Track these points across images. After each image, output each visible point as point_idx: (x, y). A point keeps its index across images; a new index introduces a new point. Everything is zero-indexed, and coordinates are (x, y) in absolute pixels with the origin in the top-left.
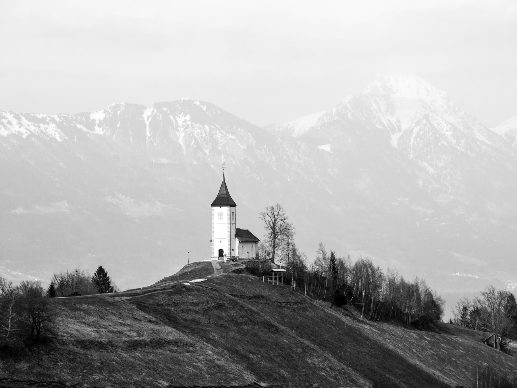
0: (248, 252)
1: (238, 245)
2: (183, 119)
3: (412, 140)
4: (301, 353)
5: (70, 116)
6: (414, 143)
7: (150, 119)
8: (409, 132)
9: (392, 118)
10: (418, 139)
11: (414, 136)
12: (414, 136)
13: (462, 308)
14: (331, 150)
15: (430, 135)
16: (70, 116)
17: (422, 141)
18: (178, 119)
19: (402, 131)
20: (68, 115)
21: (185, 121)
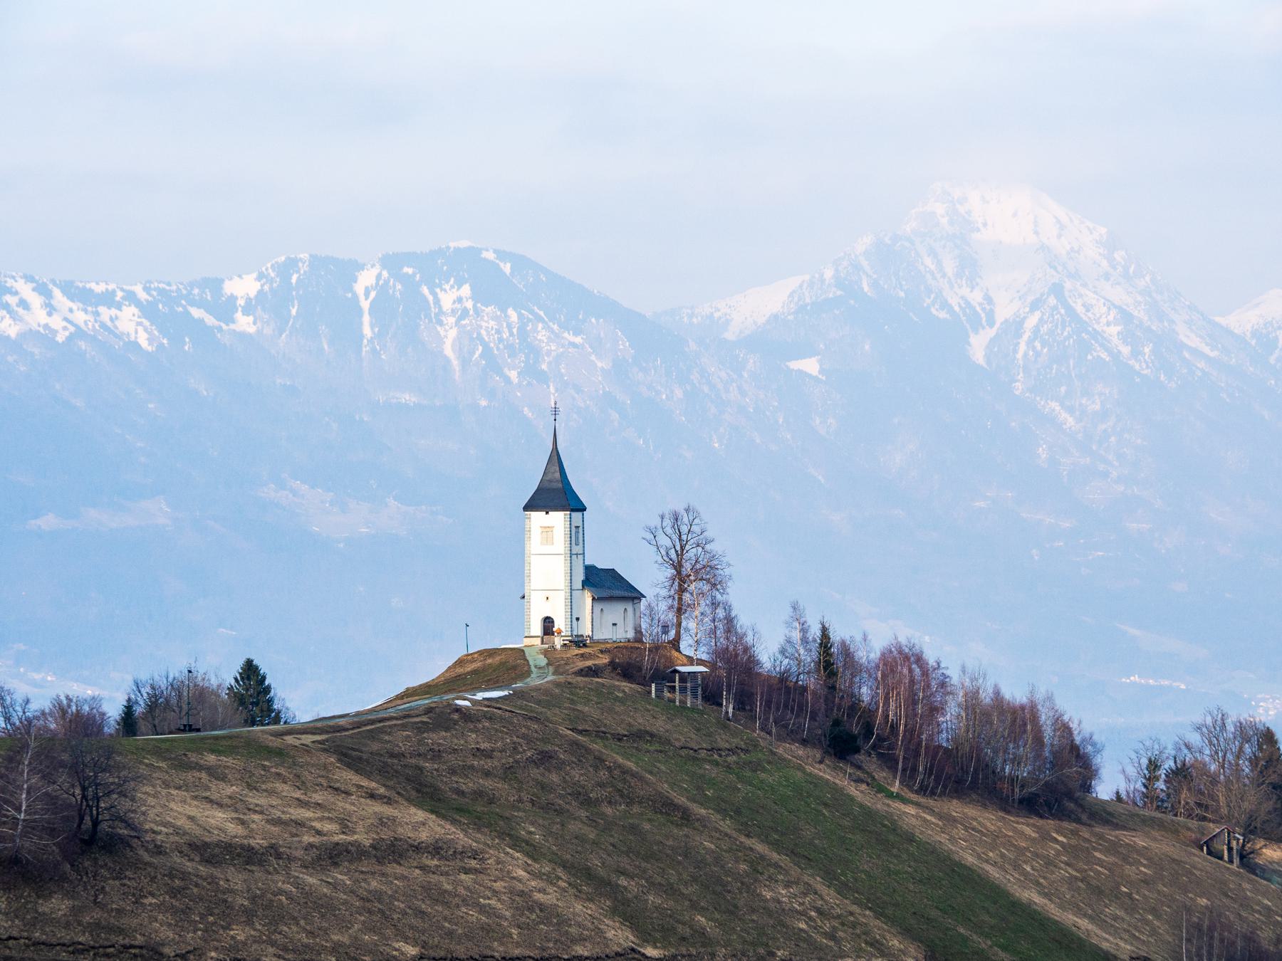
3: (1022, 348)
5: (174, 288)
6: (1026, 355)
7: (373, 294)
8: (1016, 326)
10: (1038, 345)
11: (1025, 337)
12: (1025, 337)
13: (1145, 762)
14: (820, 372)
15: (1066, 334)
16: (174, 288)
17: (1045, 350)
18: (441, 295)
21: (460, 300)
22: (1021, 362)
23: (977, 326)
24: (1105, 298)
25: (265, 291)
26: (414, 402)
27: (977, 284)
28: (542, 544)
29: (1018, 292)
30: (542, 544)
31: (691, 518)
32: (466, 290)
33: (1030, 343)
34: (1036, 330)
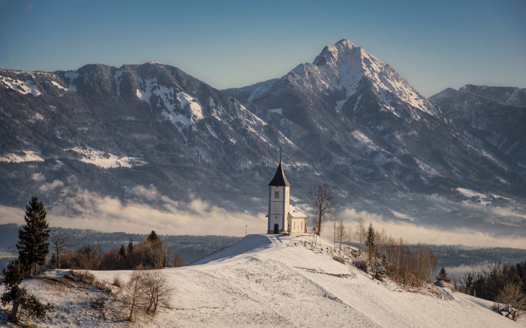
0: (298, 227)
1: (334, 274)
2: (151, 81)
3: (356, 106)
4: (200, 180)
5: (46, 74)
6: (357, 109)
7: (121, 80)
8: (353, 99)
9: (338, 86)
10: (361, 106)
11: (357, 103)
12: (357, 103)
13: (467, 277)
14: (282, 114)
15: (372, 102)
16: (46, 74)
17: (364, 108)
18: (146, 81)
19: (347, 98)
20: (44, 72)
21: (153, 83)
22: (355, 112)
23: (340, 99)
24: (417, 93)
25: (378, 149)
26: (398, 194)
27: (340, 83)
28: (275, 198)
29: (355, 86)
30: (275, 198)
31: (325, 189)
32: (155, 79)
33: (358, 105)
34: (361, 100)
